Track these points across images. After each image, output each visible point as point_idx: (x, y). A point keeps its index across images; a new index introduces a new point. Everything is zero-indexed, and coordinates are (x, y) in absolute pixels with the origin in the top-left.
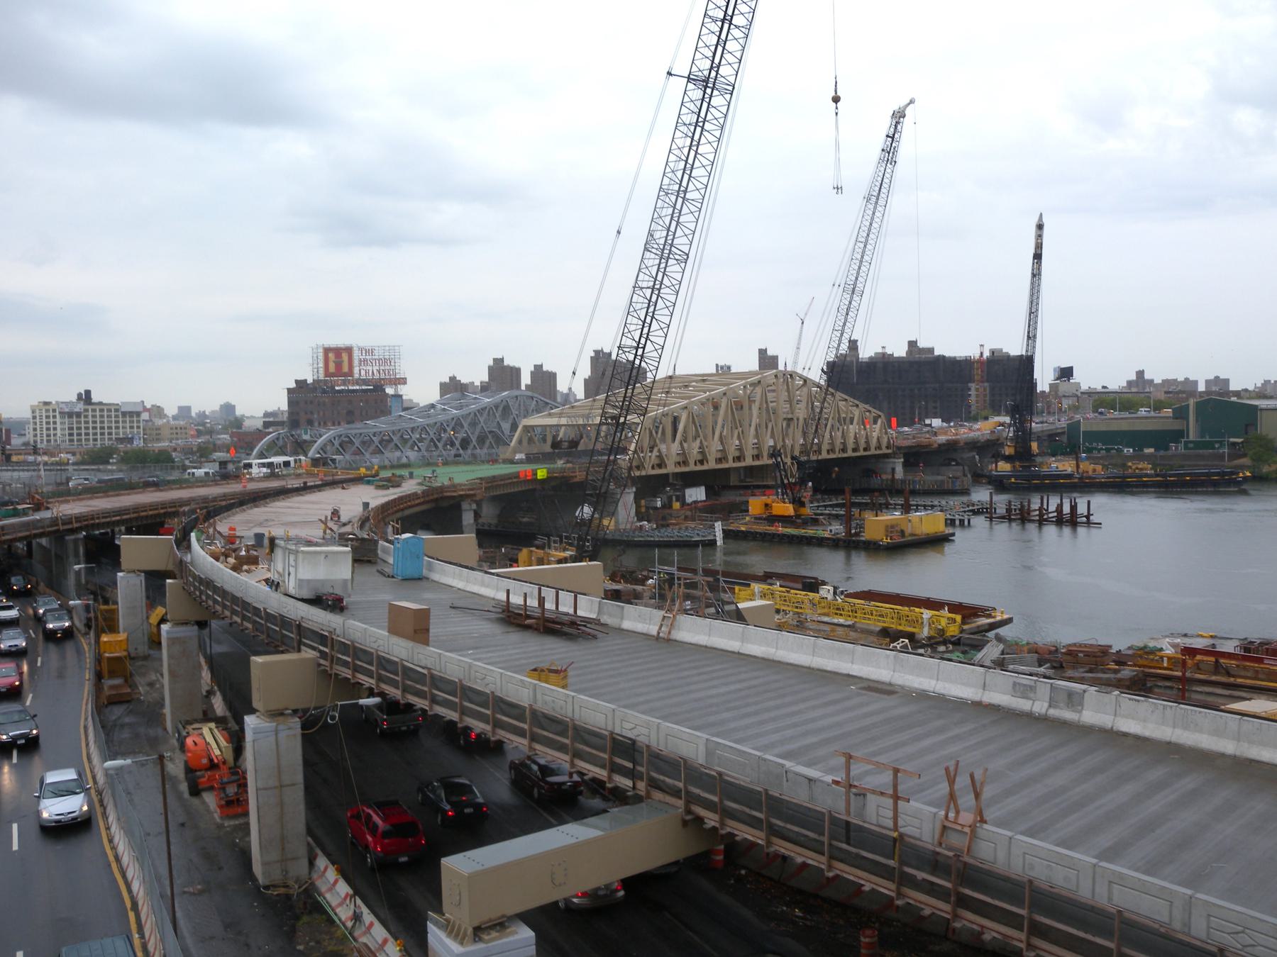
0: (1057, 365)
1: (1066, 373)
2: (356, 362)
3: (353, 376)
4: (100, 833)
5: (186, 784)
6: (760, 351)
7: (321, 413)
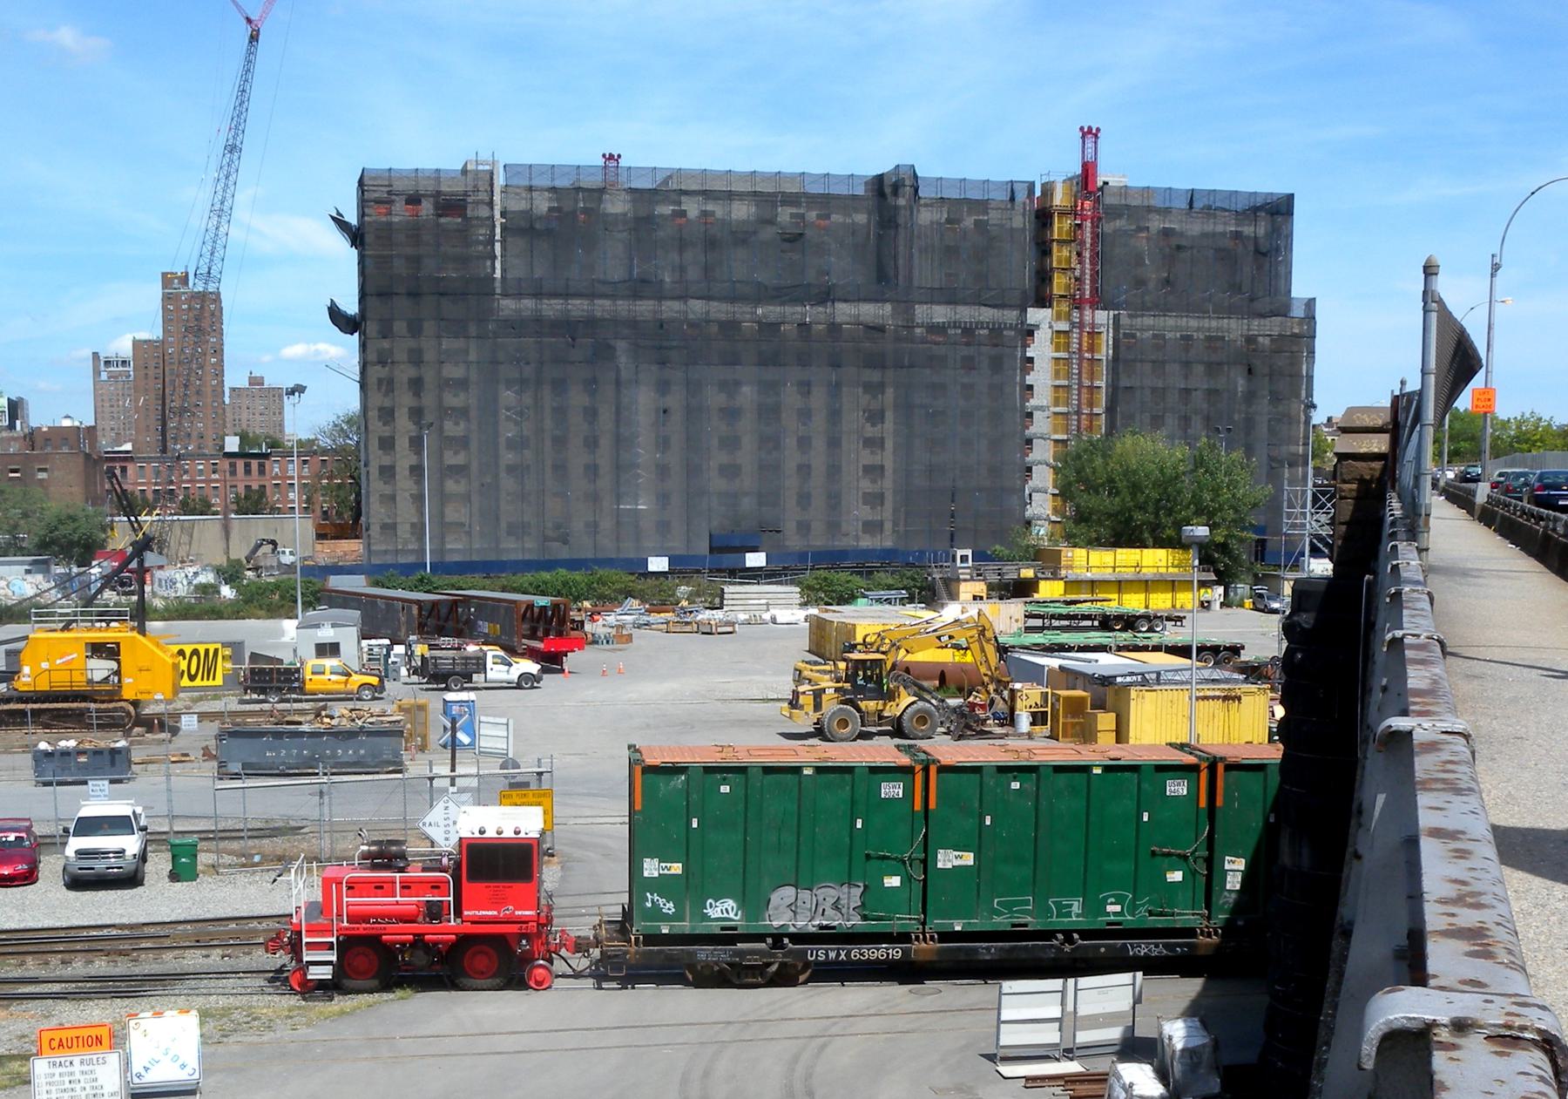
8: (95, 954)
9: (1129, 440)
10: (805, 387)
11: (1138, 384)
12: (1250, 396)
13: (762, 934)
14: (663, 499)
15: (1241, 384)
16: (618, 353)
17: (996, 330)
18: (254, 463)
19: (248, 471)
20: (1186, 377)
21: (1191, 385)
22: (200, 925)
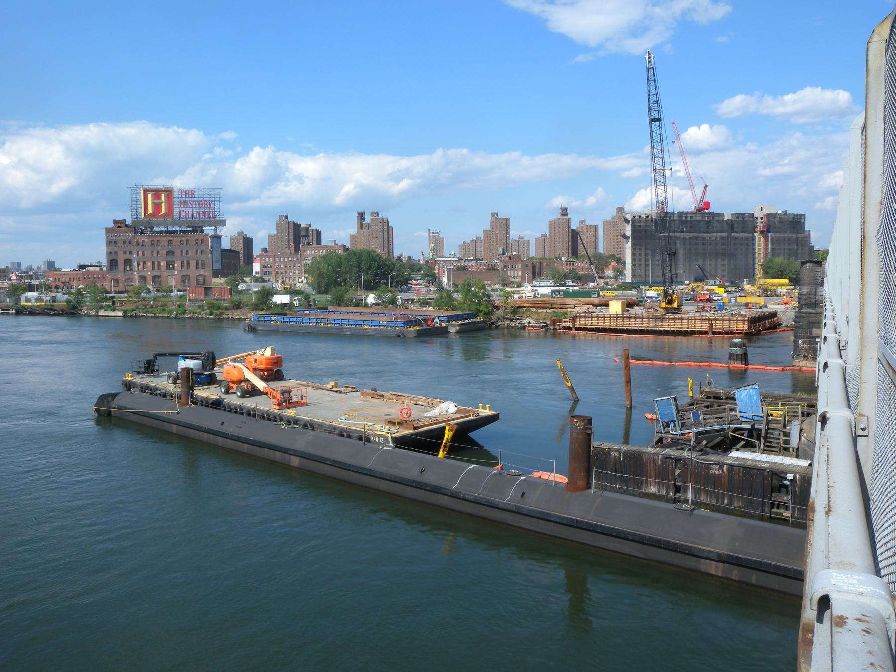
0: (599, 225)
1: (583, 222)
2: (176, 204)
3: (173, 217)
4: (522, 507)
5: (841, 91)
6: (493, 214)
7: (141, 253)
8: (518, 474)
9: (649, 196)
12: (797, 250)
13: (766, 421)
15: (796, 247)
17: (747, 239)
18: (572, 263)
19: (570, 265)
22: (665, 338)
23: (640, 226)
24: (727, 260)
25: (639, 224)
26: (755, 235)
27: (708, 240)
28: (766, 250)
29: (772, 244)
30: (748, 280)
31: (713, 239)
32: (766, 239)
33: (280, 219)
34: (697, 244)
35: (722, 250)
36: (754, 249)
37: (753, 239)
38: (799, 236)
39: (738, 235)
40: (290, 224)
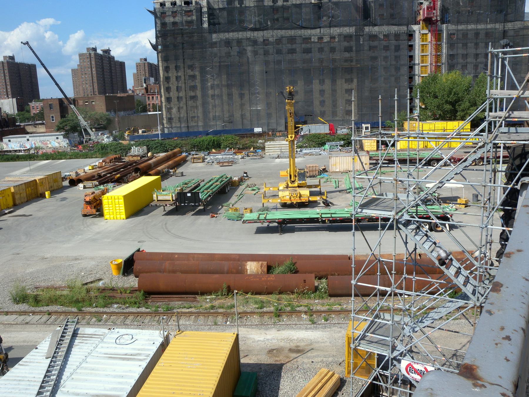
10: (322, 82)
11: (456, 53)
14: (269, 105)
16: (248, 51)
17: (397, 36)
20: (476, 49)
21: (478, 51)
23: (174, 24)
24: (355, 80)
25: (172, 20)
26: (415, 27)
27: (314, 42)
28: (438, 57)
29: (451, 45)
30: (369, 125)
31: (325, 40)
32: (438, 36)
33: (141, 61)
34: (292, 51)
35: (346, 61)
36: (411, 58)
37: (411, 36)
38: (509, 26)
39: (376, 29)
40: (4, 64)
